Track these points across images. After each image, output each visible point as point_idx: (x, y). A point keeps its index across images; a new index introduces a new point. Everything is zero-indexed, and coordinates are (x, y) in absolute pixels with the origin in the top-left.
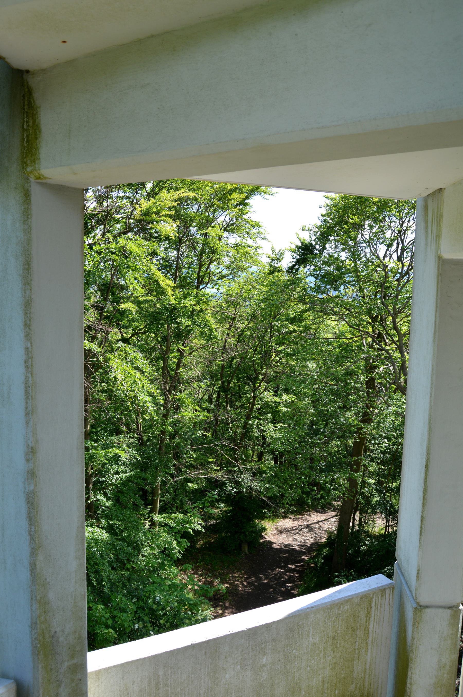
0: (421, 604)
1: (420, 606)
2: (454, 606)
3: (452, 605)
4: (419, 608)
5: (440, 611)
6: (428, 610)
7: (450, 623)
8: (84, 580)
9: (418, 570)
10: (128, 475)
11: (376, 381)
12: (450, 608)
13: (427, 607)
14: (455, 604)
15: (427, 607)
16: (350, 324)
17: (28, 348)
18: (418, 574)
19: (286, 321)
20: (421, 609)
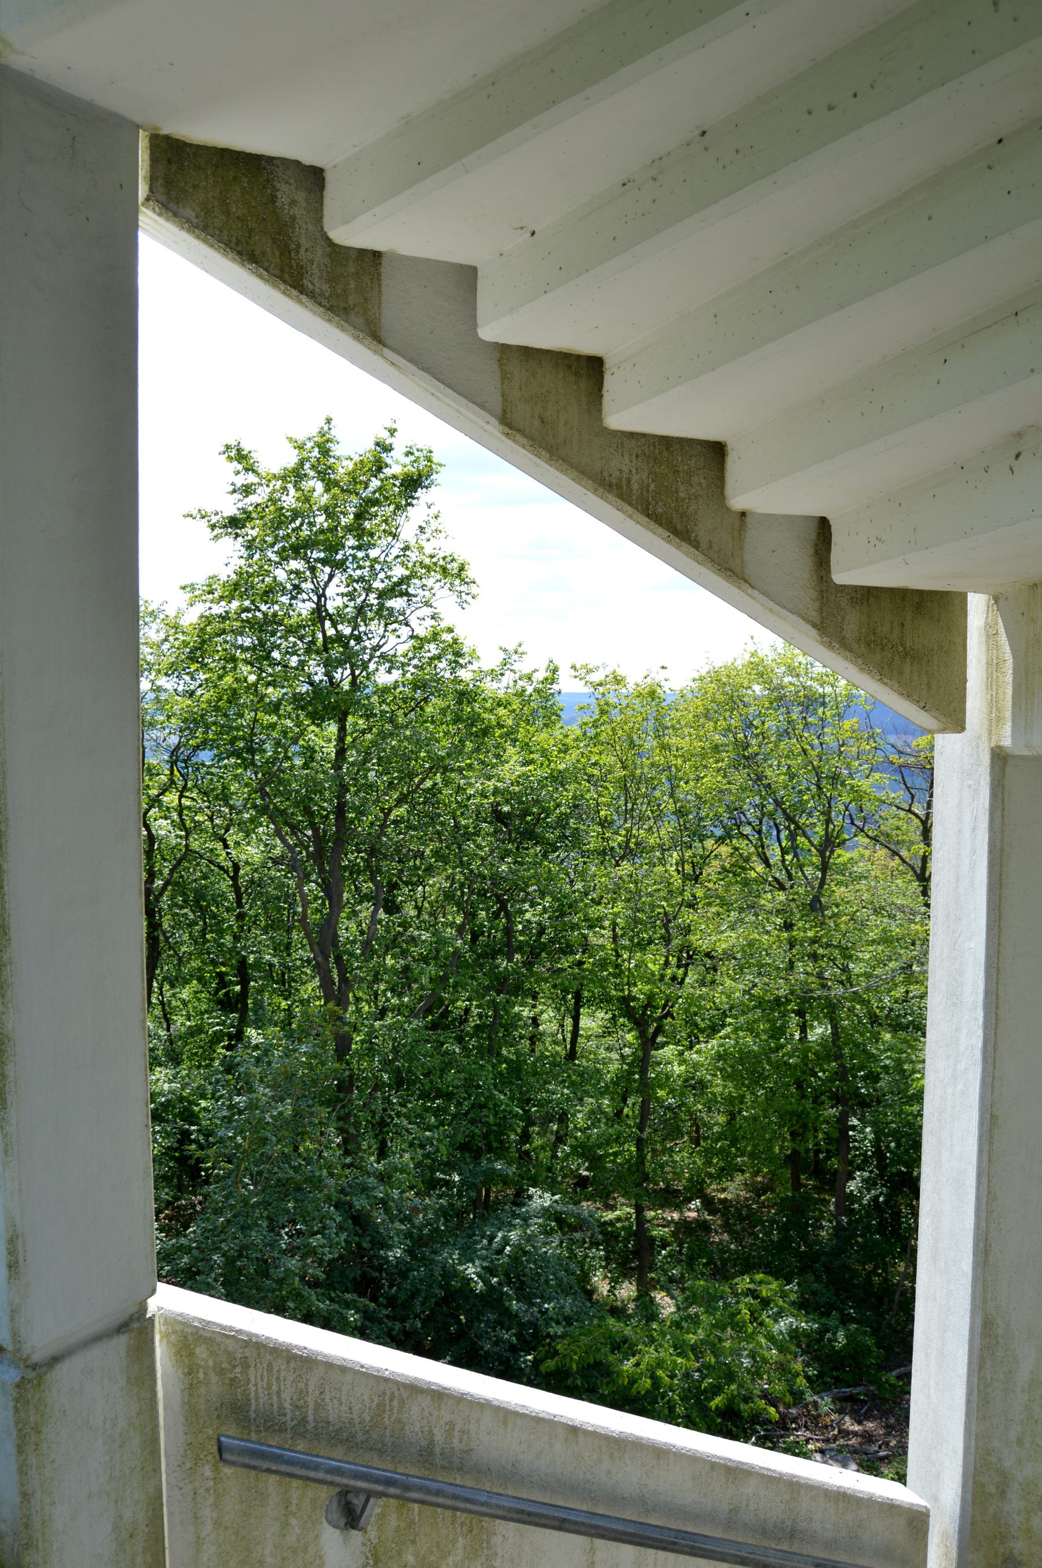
0: (36, 1358)
1: (34, 1367)
2: (131, 1319)
3: (125, 1316)
4: (32, 1375)
5: (97, 1352)
6: (63, 1372)
7: (128, 1380)
8: (976, 1008)
9: (12, 1241)
10: (829, 1027)
11: (252, 983)
12: (122, 1328)
13: (55, 1360)
14: (134, 1309)
15: (55, 1360)
16: (746, 842)
17: (388, 449)
18: (12, 1252)
19: (338, 803)
20: (40, 1377)
